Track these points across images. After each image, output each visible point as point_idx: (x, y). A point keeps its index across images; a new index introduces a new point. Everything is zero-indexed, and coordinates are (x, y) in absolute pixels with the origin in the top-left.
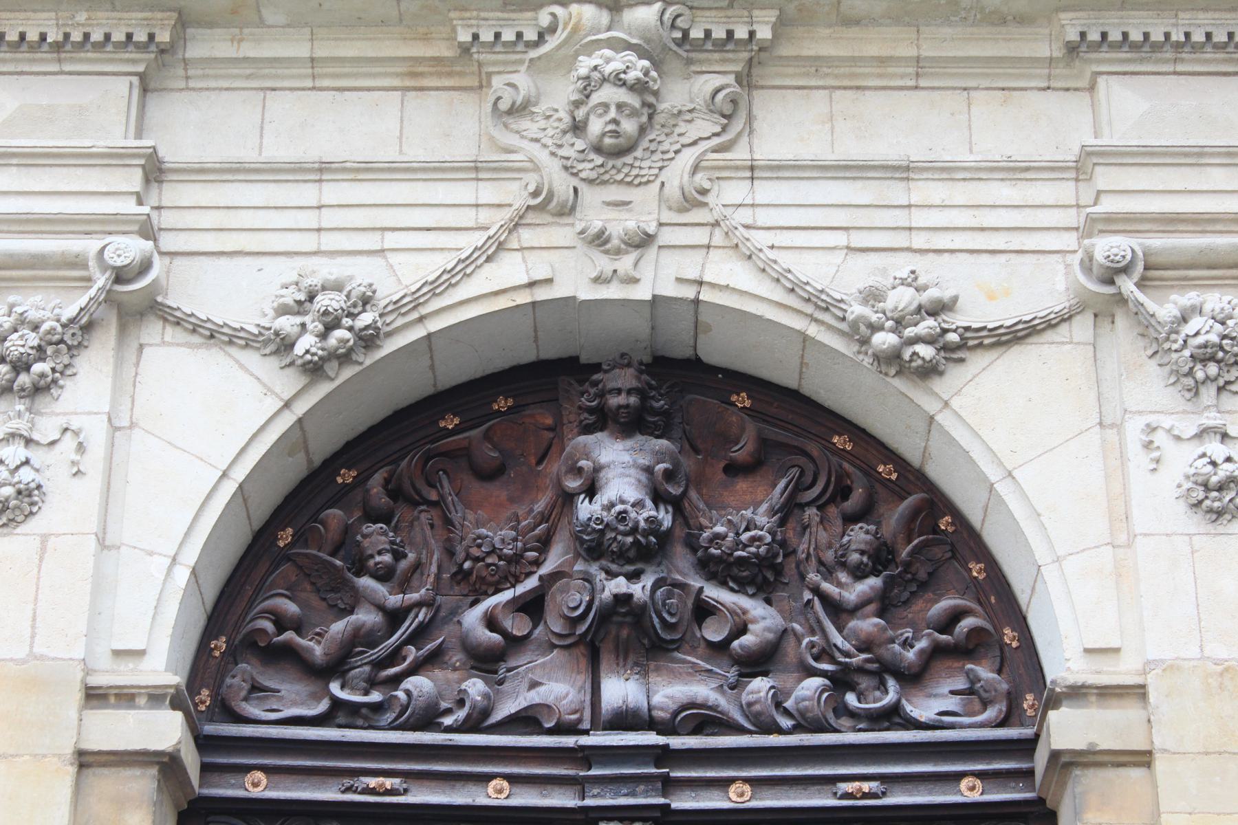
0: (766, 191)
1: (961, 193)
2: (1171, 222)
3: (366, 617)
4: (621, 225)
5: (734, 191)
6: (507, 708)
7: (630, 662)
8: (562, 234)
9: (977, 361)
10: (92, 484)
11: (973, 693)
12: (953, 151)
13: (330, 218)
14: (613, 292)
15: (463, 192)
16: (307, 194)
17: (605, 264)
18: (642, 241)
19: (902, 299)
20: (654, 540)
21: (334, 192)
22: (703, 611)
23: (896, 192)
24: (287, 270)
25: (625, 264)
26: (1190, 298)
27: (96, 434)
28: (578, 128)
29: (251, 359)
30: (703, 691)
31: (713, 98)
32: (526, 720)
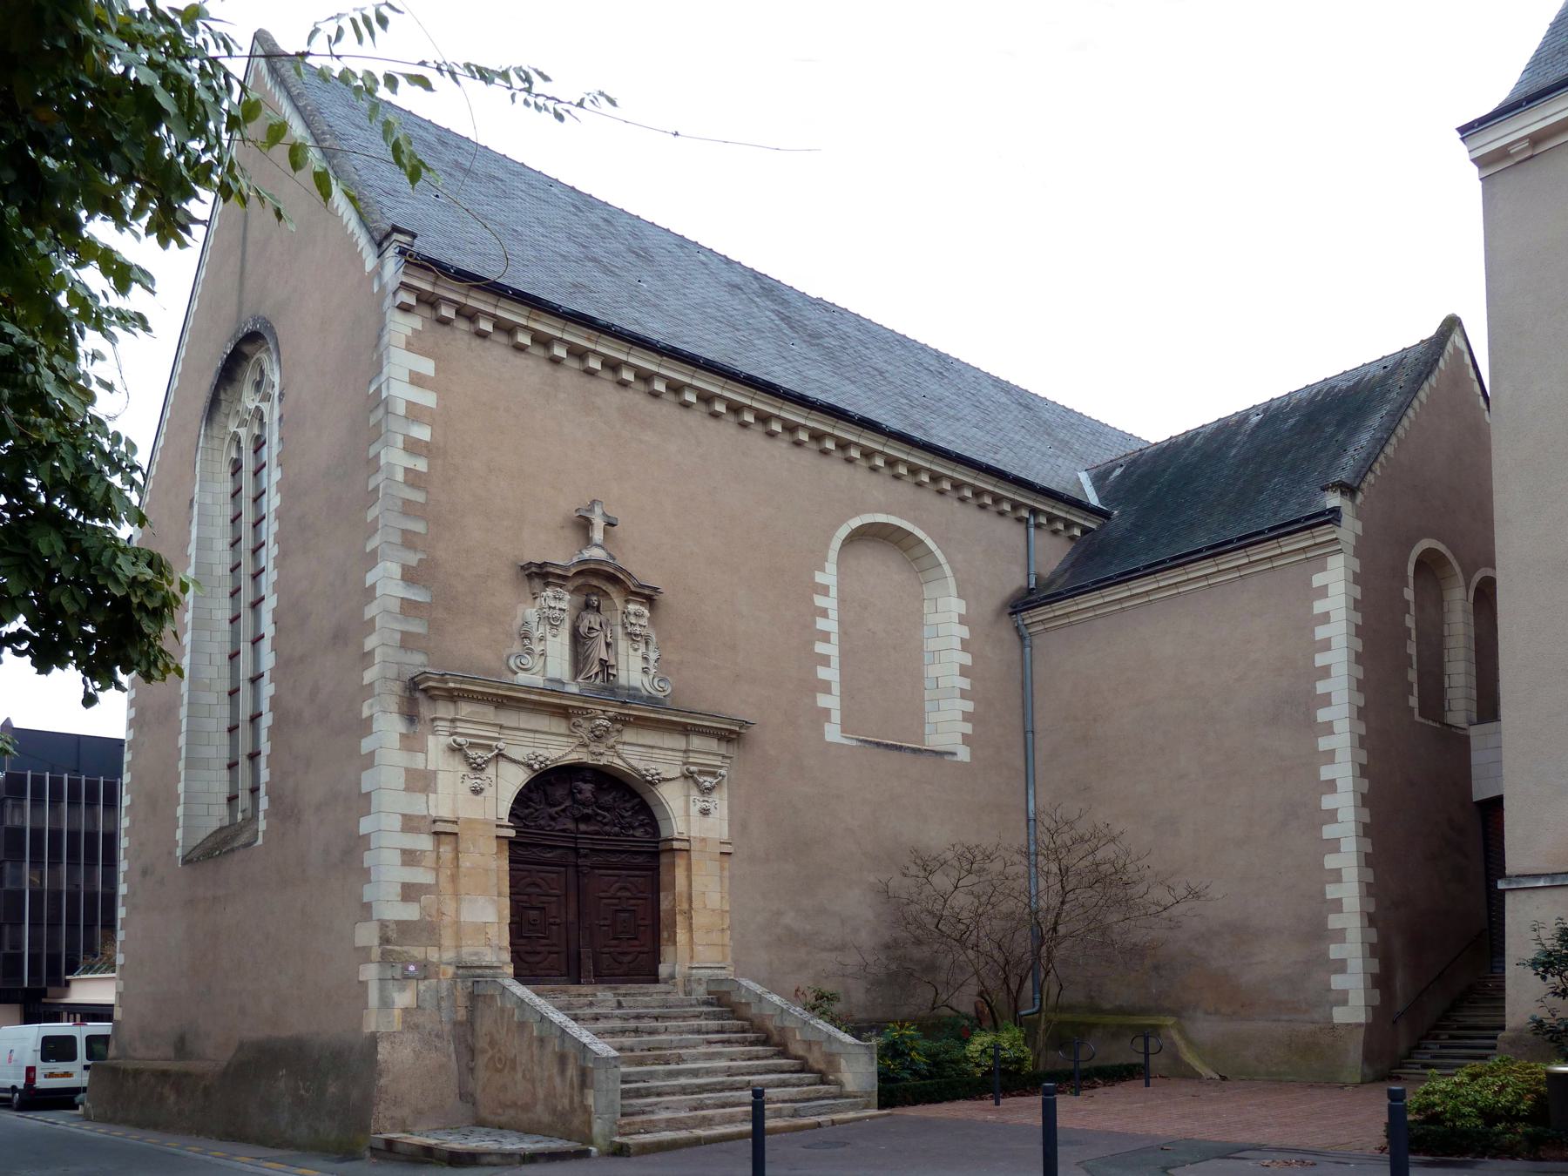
0: (626, 747)
1: (662, 752)
2: (702, 764)
3: (532, 810)
4: (596, 750)
5: (619, 747)
6: (557, 828)
7: (147, 626)
8: (585, 750)
9: (662, 783)
10: (494, 788)
11: (646, 832)
12: (660, 744)
13: (536, 740)
14: (595, 762)
15: (565, 739)
16: (532, 735)
17: (595, 757)
18: (601, 754)
19: (654, 772)
20: (32, 512)
21: (537, 736)
22: (598, 814)
23: (650, 751)
24: (530, 751)
25: (599, 757)
26: (705, 778)
27: (494, 778)
28: (592, 732)
29: (522, 767)
30: (596, 828)
31: (947, 1006)
32: (564, 831)
